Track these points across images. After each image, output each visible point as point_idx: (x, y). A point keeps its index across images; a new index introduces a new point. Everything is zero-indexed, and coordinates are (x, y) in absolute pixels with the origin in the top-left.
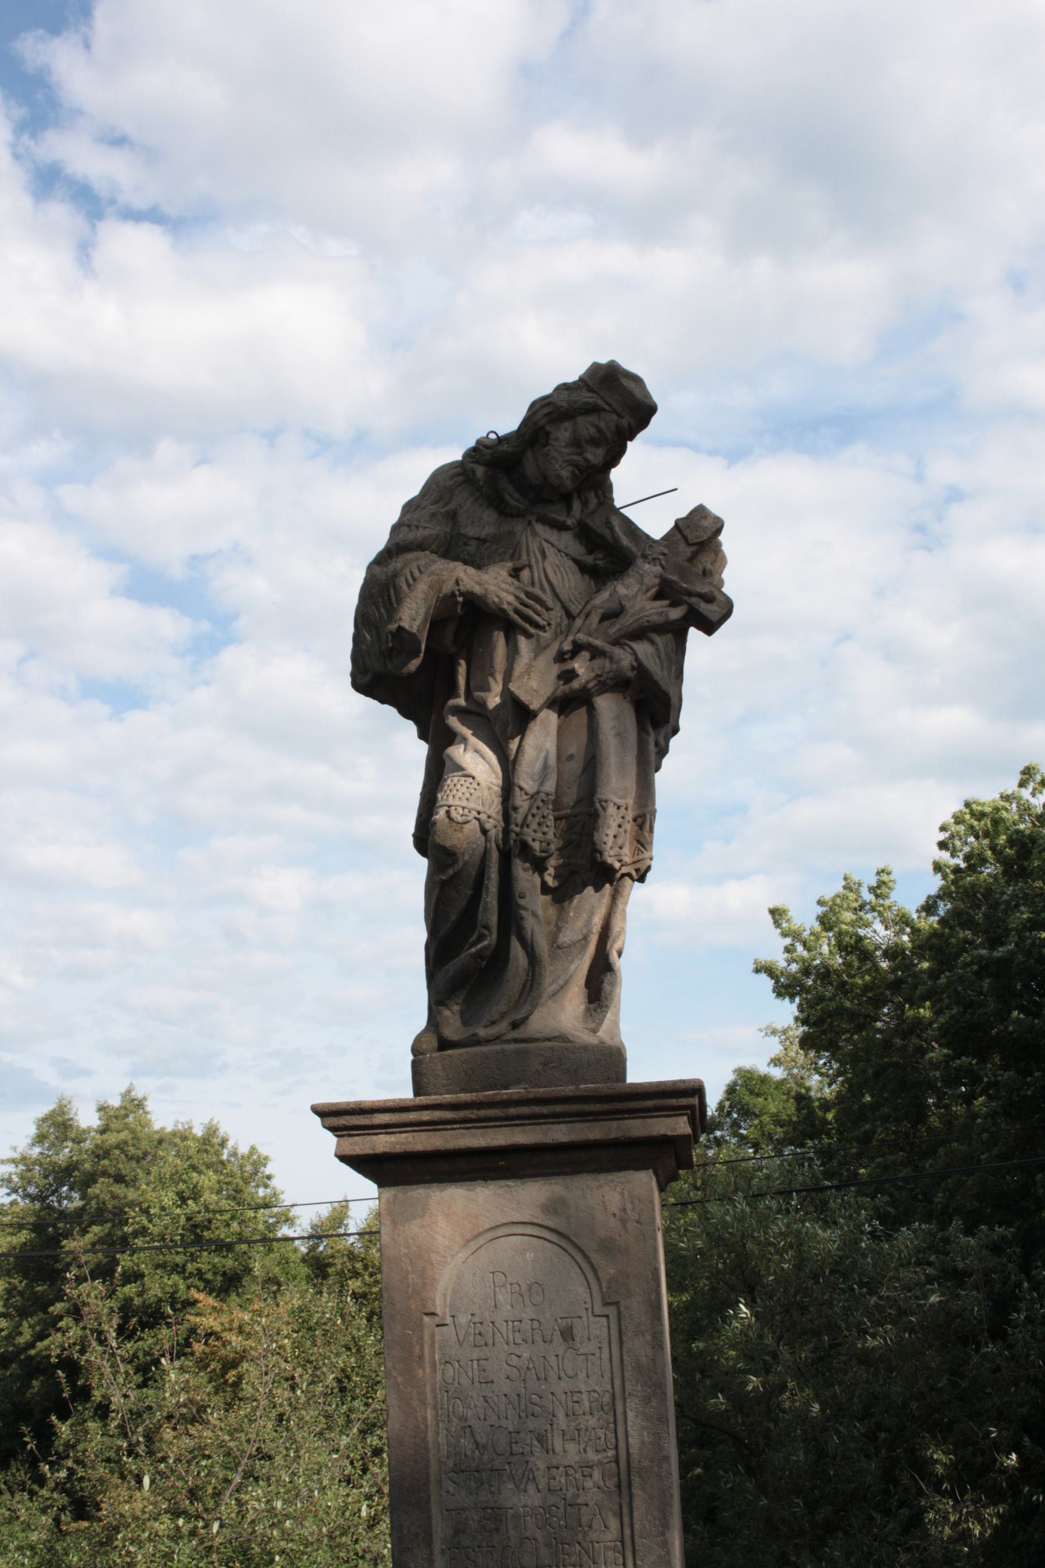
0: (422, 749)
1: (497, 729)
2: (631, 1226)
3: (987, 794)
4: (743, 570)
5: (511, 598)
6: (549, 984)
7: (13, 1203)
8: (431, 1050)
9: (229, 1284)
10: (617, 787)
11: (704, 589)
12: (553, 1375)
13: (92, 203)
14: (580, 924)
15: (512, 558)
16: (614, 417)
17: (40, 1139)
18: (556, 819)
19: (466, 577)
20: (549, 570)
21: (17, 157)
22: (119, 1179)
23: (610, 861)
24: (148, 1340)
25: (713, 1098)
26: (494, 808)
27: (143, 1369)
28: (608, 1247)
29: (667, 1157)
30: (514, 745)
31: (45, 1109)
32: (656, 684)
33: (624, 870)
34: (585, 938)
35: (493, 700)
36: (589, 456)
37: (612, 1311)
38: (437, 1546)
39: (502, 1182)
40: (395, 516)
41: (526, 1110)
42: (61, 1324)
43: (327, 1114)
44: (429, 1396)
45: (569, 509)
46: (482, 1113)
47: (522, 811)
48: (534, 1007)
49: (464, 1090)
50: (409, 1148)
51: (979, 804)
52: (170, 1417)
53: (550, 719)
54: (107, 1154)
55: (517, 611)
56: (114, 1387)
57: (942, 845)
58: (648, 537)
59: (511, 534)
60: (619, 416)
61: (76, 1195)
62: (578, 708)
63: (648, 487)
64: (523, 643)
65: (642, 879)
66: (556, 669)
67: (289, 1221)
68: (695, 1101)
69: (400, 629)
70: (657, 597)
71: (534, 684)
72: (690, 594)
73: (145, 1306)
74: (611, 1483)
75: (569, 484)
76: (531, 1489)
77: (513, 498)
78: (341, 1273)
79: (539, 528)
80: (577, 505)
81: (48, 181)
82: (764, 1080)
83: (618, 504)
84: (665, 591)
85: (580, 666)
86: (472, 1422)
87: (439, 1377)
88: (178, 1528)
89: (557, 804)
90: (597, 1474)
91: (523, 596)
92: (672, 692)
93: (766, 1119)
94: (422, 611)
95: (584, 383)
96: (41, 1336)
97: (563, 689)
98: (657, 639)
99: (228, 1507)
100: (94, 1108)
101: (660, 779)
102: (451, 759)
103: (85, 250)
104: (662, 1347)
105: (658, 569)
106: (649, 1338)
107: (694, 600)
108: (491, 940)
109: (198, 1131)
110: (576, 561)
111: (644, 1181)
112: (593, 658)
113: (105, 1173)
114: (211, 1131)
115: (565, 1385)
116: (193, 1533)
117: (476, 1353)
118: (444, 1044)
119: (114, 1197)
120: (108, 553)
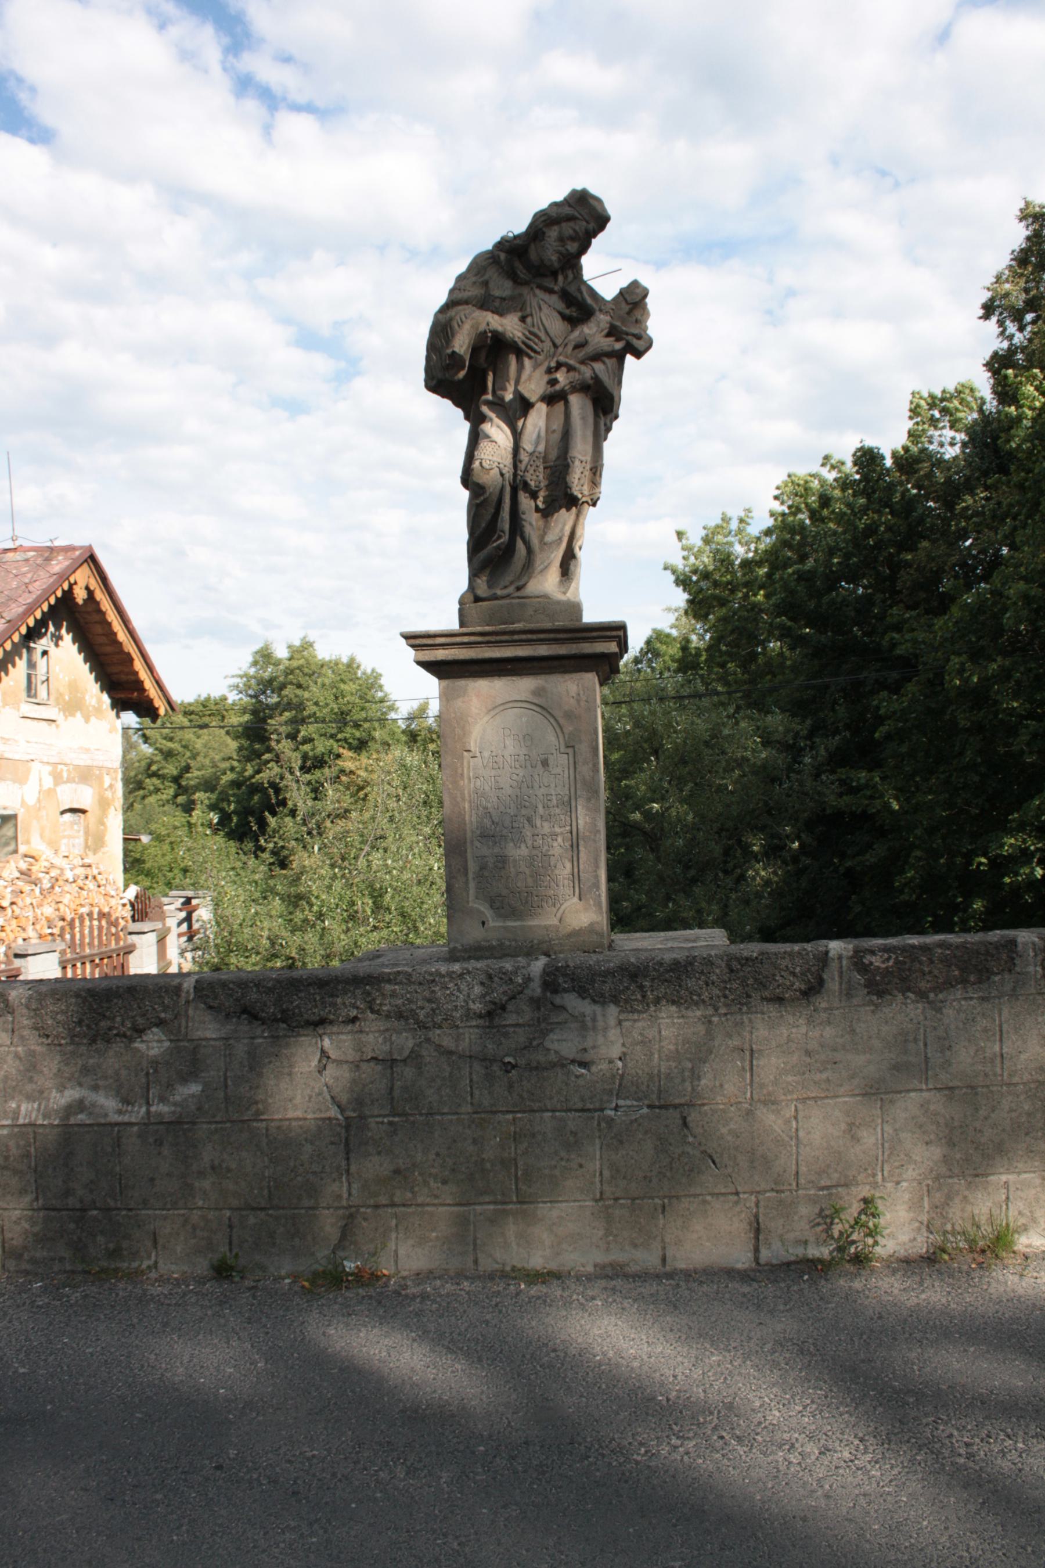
0: (467, 426)
1: (511, 413)
2: (582, 704)
3: (802, 471)
4: (659, 322)
5: (520, 334)
6: (538, 565)
7: (241, 699)
8: (470, 601)
9: (360, 746)
10: (581, 450)
11: (635, 331)
12: (536, 785)
13: (271, 99)
14: (557, 530)
15: (521, 310)
16: (584, 223)
17: (255, 663)
18: (545, 468)
19: (493, 321)
20: (543, 318)
21: (225, 69)
22: (299, 686)
23: (576, 493)
24: (317, 774)
25: (636, 642)
26: (508, 460)
27: (315, 790)
28: (569, 715)
29: (606, 666)
30: (520, 423)
31: (257, 647)
32: (605, 388)
33: (584, 499)
34: (560, 539)
35: (509, 396)
36: (569, 248)
37: (570, 751)
38: (471, 875)
39: (509, 678)
40: (451, 284)
41: (524, 637)
42: (269, 766)
43: (408, 637)
44: (467, 795)
45: (556, 280)
46: (498, 638)
47: (525, 463)
48: (530, 578)
49: (488, 625)
50: (456, 658)
51: (795, 476)
52: (329, 816)
53: (541, 408)
54: (292, 672)
55: (523, 343)
56: (298, 797)
57: (776, 498)
58: (603, 299)
59: (521, 295)
60: (587, 222)
61: (275, 695)
62: (558, 401)
63: (603, 270)
64: (527, 362)
65: (594, 505)
66: (546, 378)
67: (392, 708)
68: (621, 633)
69: (454, 352)
70: (608, 335)
71: (533, 386)
72: (627, 334)
73: (315, 758)
74: (568, 844)
75: (556, 265)
76: (523, 846)
77: (522, 273)
78: (424, 740)
79: (538, 292)
80: (560, 278)
81: (245, 85)
82: (668, 636)
83: (586, 277)
84: (613, 332)
85: (561, 376)
86: (491, 810)
87: (472, 785)
88: (335, 874)
89: (545, 459)
90: (560, 839)
91: (527, 333)
92: (615, 394)
93: (667, 658)
94: (467, 341)
95: (567, 202)
96: (258, 772)
97: (550, 390)
98: (607, 360)
99: (362, 862)
100: (285, 646)
101: (607, 445)
102: (483, 431)
103: (267, 130)
104: (598, 771)
105: (608, 318)
106: (591, 765)
107: (630, 338)
108: (505, 539)
109: (345, 660)
110: (560, 313)
111: (591, 679)
112: (568, 371)
113: (291, 683)
114: (352, 660)
115: (543, 791)
116: (343, 876)
117: (493, 773)
118: (477, 599)
119: (296, 696)
120: (286, 321)
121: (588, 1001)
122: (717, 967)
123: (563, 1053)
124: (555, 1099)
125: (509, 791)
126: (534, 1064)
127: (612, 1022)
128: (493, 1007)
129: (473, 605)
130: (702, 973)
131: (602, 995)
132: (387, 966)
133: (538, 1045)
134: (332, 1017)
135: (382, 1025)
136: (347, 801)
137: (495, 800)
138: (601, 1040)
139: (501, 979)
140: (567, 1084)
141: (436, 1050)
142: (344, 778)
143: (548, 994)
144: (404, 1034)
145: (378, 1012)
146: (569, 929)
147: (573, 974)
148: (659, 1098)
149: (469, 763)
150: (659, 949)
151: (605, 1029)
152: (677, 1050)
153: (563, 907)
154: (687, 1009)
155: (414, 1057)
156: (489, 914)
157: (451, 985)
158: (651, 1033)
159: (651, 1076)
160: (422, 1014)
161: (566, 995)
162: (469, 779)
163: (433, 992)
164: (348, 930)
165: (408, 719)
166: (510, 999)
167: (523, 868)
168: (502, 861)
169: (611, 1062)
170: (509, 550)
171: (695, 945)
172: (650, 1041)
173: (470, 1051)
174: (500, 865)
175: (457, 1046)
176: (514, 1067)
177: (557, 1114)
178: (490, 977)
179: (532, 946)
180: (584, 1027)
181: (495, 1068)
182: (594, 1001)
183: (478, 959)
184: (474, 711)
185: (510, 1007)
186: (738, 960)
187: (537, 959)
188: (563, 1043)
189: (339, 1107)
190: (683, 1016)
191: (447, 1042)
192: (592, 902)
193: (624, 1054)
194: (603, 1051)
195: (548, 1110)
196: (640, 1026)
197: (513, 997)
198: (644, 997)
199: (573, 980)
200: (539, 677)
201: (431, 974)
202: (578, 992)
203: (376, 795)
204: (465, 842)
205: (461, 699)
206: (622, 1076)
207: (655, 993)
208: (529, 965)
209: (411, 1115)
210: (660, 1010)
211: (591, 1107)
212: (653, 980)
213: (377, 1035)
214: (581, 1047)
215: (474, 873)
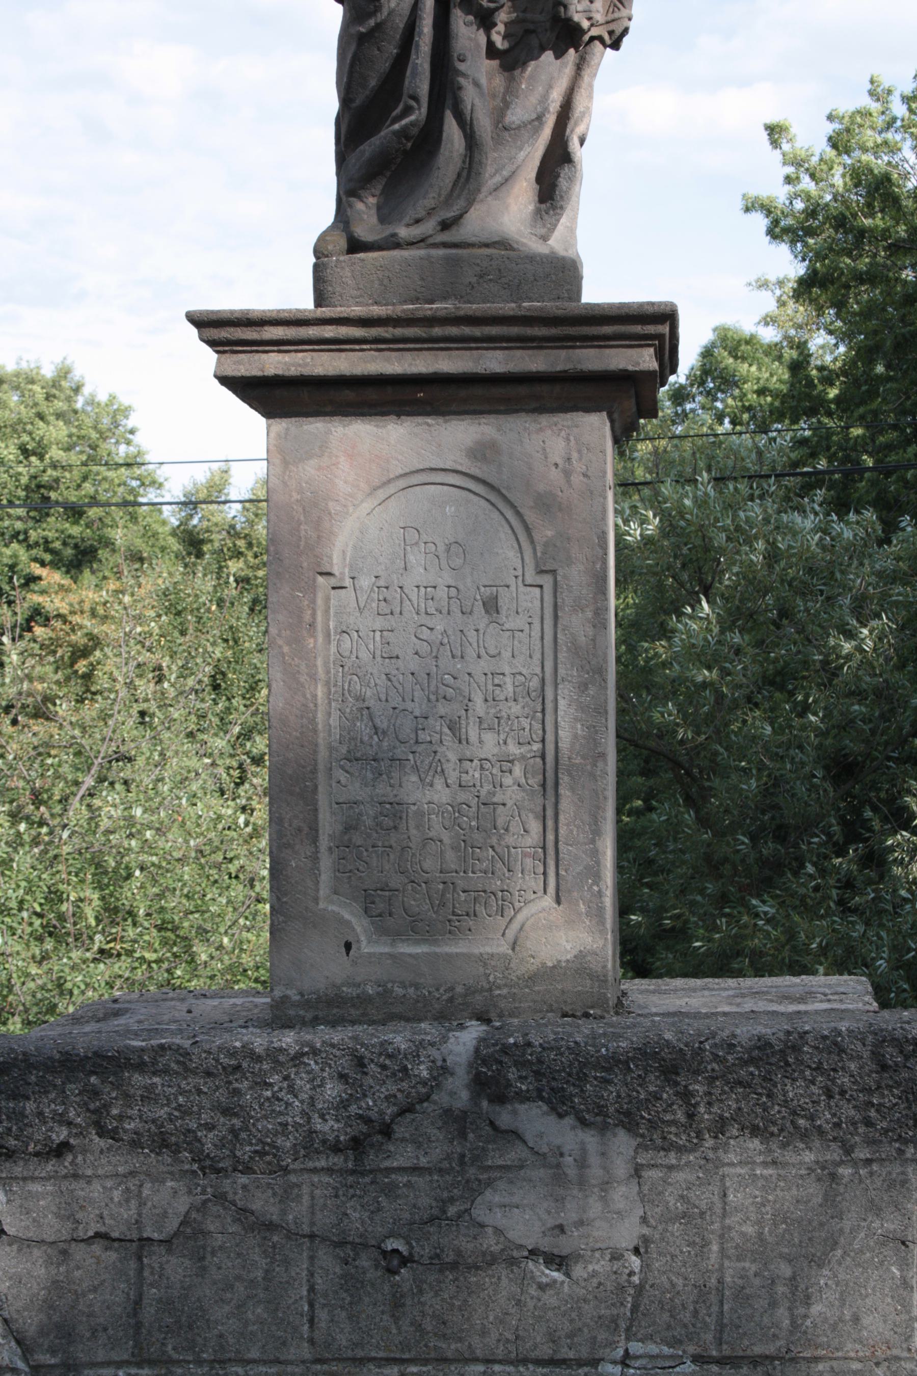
2: (577, 479)
6: (490, 177)
8: (344, 242)
9: (80, 559)
12: (471, 653)
14: (533, 99)
23: (576, 18)
29: (629, 399)
33: (594, 32)
34: (540, 118)
37: (547, 581)
38: (324, 842)
39: (420, 419)
41: (453, 331)
43: (205, 323)
44: (320, 670)
48: (470, 203)
50: (307, 371)
65: (616, 45)
68: (665, 329)
76: (439, 783)
86: (371, 703)
87: (333, 649)
88: (19, 834)
90: (518, 770)
99: (77, 812)
106: (589, 614)
108: (419, 114)
109: (48, 372)
114: (64, 372)
115: (485, 665)
116: (35, 842)
117: (379, 623)
121: (569, 1121)
122: (851, 1058)
123: (511, 1235)
124: (494, 1335)
125: (413, 664)
126: (450, 1257)
127: (621, 1169)
128: (364, 1128)
129: (347, 257)
130: (819, 1068)
131: (601, 1110)
132: (136, 1034)
133: (460, 1215)
134: (12, 1142)
135: (122, 1163)
136: (47, 677)
137: (382, 681)
138: (595, 1208)
139: (384, 1067)
140: (518, 1303)
141: (236, 1220)
142: (39, 631)
143: (485, 1104)
144: (169, 1184)
145: (113, 1134)
146: (532, 965)
147: (540, 1061)
148: (720, 1342)
149: (327, 599)
150: (725, 1014)
151: (606, 1185)
152: (760, 1234)
153: (520, 917)
154: (784, 1146)
155: (188, 1236)
156: (359, 926)
157: (275, 1078)
158: (705, 1197)
159: (702, 1291)
160: (209, 1141)
161: (522, 1108)
162: (328, 635)
163: (237, 1092)
164: (45, 957)
165: (184, 504)
166: (402, 1113)
167: (437, 828)
168: (394, 813)
169: (616, 1256)
170: (428, 139)
171: (802, 1007)
172: (702, 1214)
173: (312, 1224)
174: (388, 822)
175: (284, 1212)
176: (405, 1261)
177: (497, 1368)
178: (360, 1063)
179: (451, 1000)
180: (559, 1178)
181: (364, 1262)
182: (584, 1123)
183: (333, 1024)
184: (342, 487)
185: (400, 1131)
186: (898, 1043)
187: (461, 1027)
188: (516, 1214)
189: (18, 1342)
190: (774, 1162)
191: (263, 1203)
192: (582, 907)
193: (646, 1240)
194: (600, 1232)
195: (476, 1360)
196: (680, 1179)
197: (407, 1109)
198: (691, 1116)
199: (537, 1073)
200: (484, 419)
201: (232, 1053)
202: (548, 1102)
203: (112, 667)
204: (314, 771)
205: (313, 462)
206: (640, 1289)
207: (715, 1109)
208: (445, 1039)
209: (178, 1362)
210: (726, 1147)
211: (571, 1355)
212: (711, 1080)
213: (109, 1184)
214: (551, 1223)
215: (332, 837)
